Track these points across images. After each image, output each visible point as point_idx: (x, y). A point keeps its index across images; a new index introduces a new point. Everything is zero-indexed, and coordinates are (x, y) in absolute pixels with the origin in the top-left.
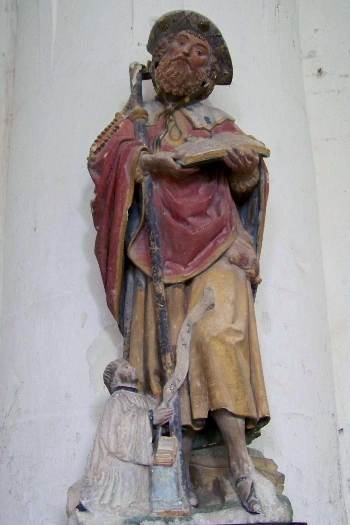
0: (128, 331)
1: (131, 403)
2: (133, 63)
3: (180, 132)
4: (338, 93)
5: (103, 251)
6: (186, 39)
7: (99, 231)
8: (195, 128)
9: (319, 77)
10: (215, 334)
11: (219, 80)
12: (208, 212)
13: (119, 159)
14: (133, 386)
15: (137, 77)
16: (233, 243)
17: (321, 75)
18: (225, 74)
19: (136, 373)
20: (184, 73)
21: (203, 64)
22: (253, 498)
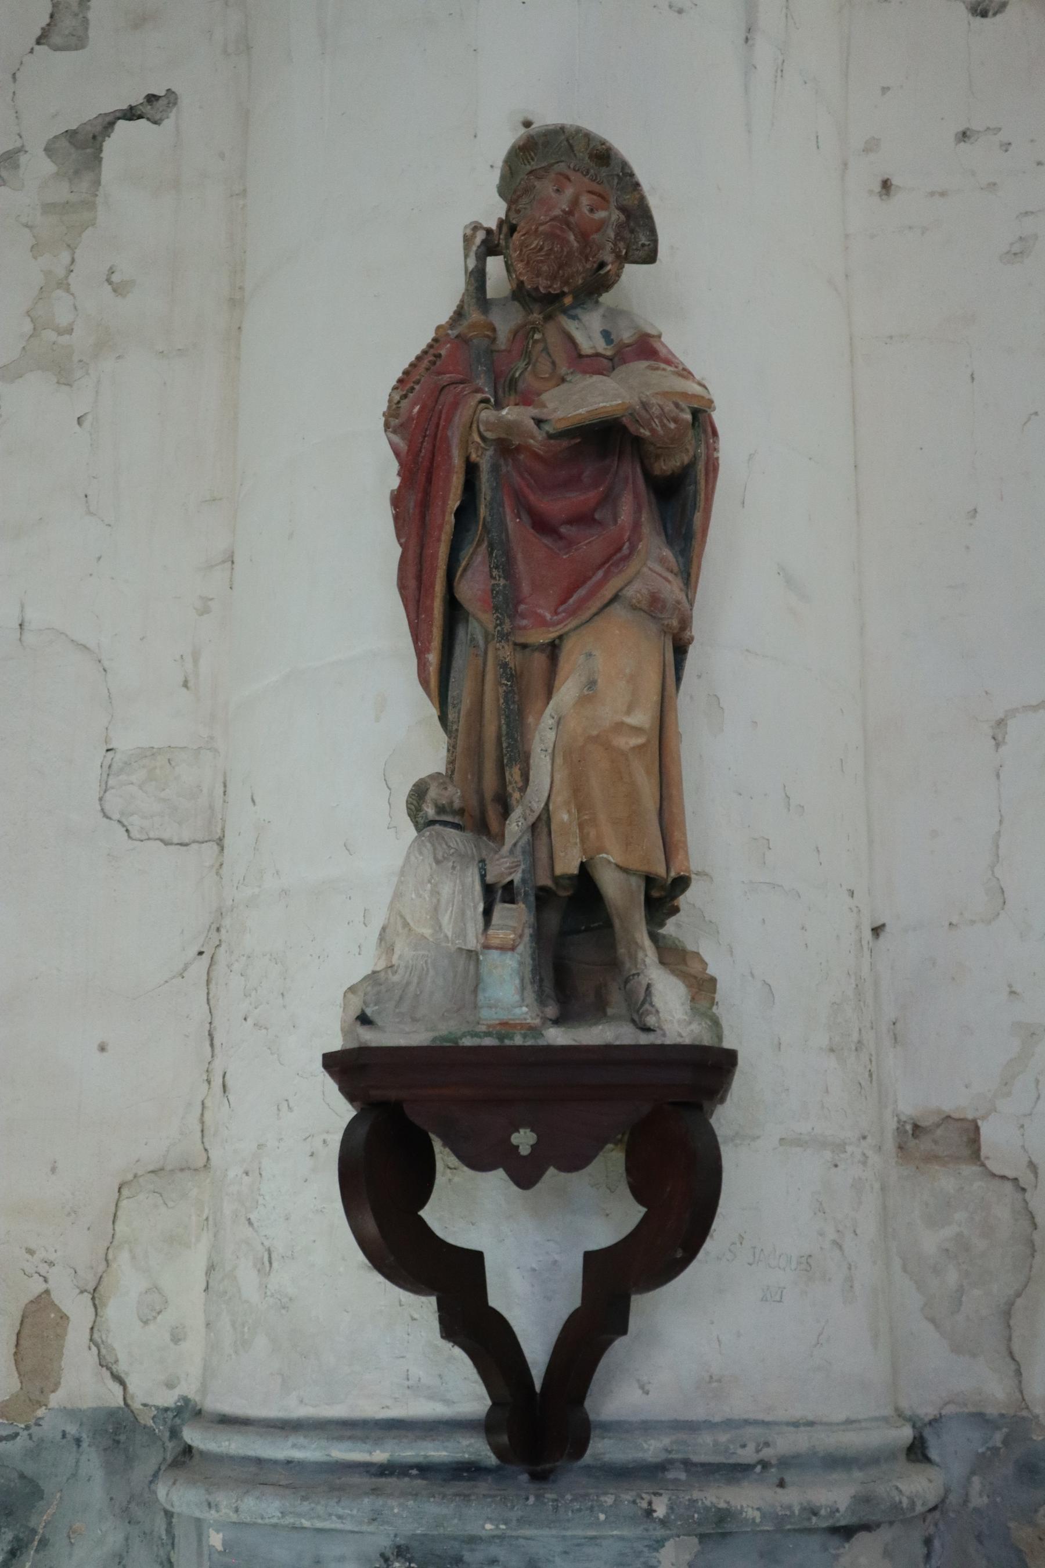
0: (455, 727)
1: (449, 846)
2: (471, 223)
3: (554, 363)
4: (923, 233)
5: (412, 583)
7: (404, 546)
8: (580, 356)
9: (884, 197)
10: (595, 733)
12: (597, 516)
13: (439, 418)
14: (457, 820)
16: (638, 572)
17: (888, 194)
18: (643, 245)
19: (462, 797)
21: (601, 225)
22: (647, 1006)
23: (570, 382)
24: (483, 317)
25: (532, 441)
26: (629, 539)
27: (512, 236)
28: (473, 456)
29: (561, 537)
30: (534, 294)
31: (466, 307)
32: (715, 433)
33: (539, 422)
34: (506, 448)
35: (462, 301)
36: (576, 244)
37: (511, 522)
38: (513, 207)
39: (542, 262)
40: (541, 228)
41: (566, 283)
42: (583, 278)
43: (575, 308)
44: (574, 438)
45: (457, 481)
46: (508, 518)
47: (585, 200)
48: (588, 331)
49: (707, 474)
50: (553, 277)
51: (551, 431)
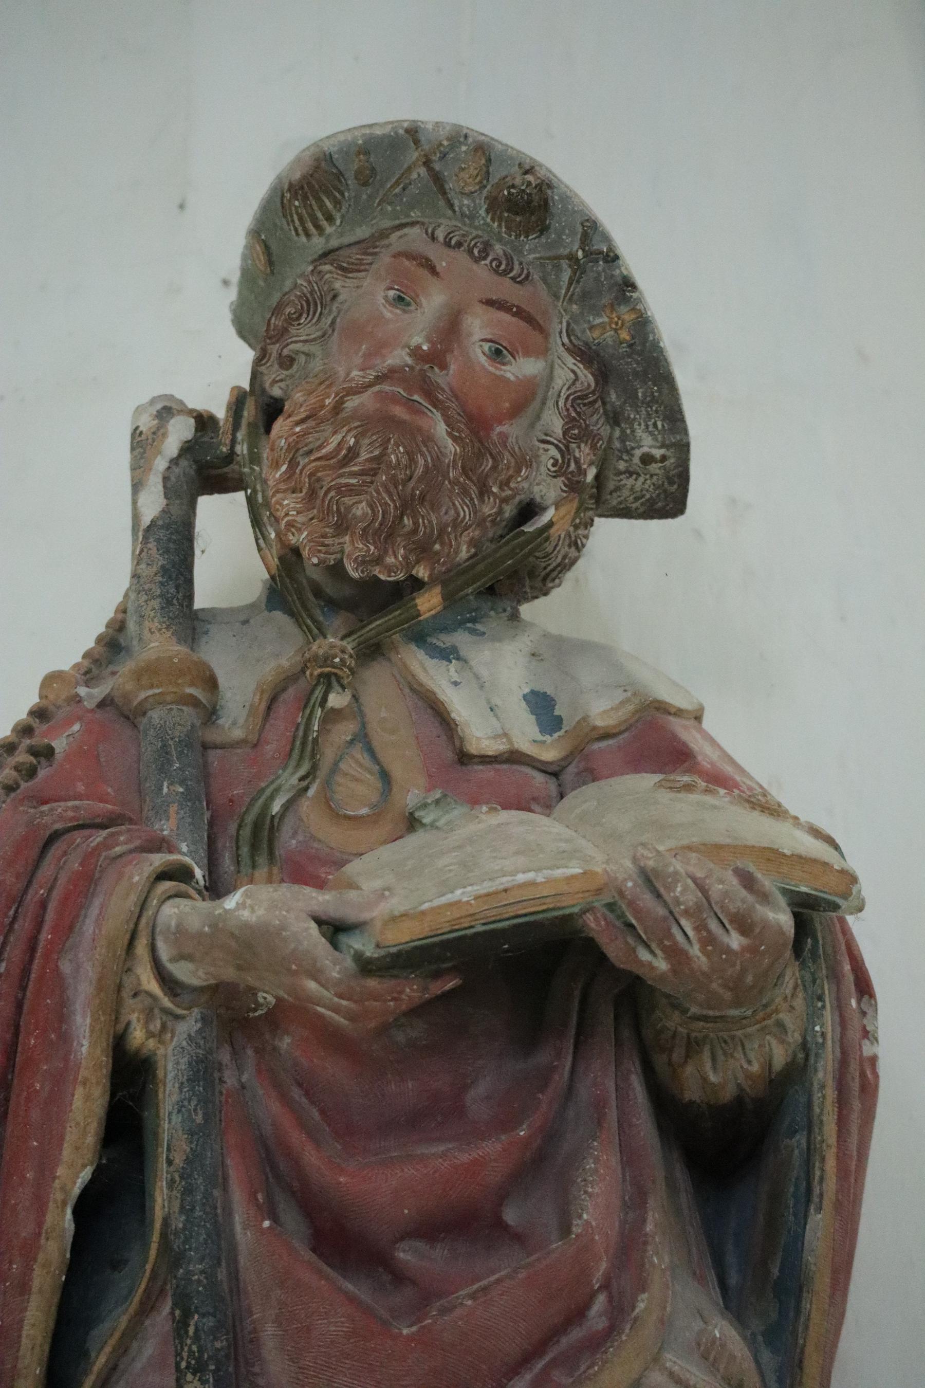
2: (153, 401)
3: (385, 776)
6: (424, 273)
8: (464, 758)
11: (618, 489)
12: (510, 1216)
13: (39, 924)
15: (166, 479)
18: (647, 459)
20: (412, 460)
21: (525, 399)
23: (433, 825)
24: (183, 649)
25: (312, 985)
26: (606, 1286)
27: (268, 431)
28: (137, 1036)
29: (399, 1277)
30: (330, 589)
31: (131, 626)
32: (864, 988)
33: (335, 929)
34: (235, 1016)
35: (122, 610)
36: (451, 447)
37: (246, 1230)
38: (274, 349)
39: (351, 490)
40: (352, 403)
41: (422, 550)
42: (472, 543)
43: (445, 629)
44: (437, 975)
45: (85, 1107)
46: (238, 1220)
47: (479, 327)
48: (488, 688)
49: (842, 1102)
50: (385, 534)
51: (370, 952)
